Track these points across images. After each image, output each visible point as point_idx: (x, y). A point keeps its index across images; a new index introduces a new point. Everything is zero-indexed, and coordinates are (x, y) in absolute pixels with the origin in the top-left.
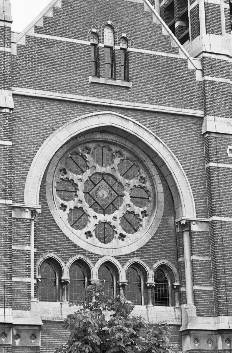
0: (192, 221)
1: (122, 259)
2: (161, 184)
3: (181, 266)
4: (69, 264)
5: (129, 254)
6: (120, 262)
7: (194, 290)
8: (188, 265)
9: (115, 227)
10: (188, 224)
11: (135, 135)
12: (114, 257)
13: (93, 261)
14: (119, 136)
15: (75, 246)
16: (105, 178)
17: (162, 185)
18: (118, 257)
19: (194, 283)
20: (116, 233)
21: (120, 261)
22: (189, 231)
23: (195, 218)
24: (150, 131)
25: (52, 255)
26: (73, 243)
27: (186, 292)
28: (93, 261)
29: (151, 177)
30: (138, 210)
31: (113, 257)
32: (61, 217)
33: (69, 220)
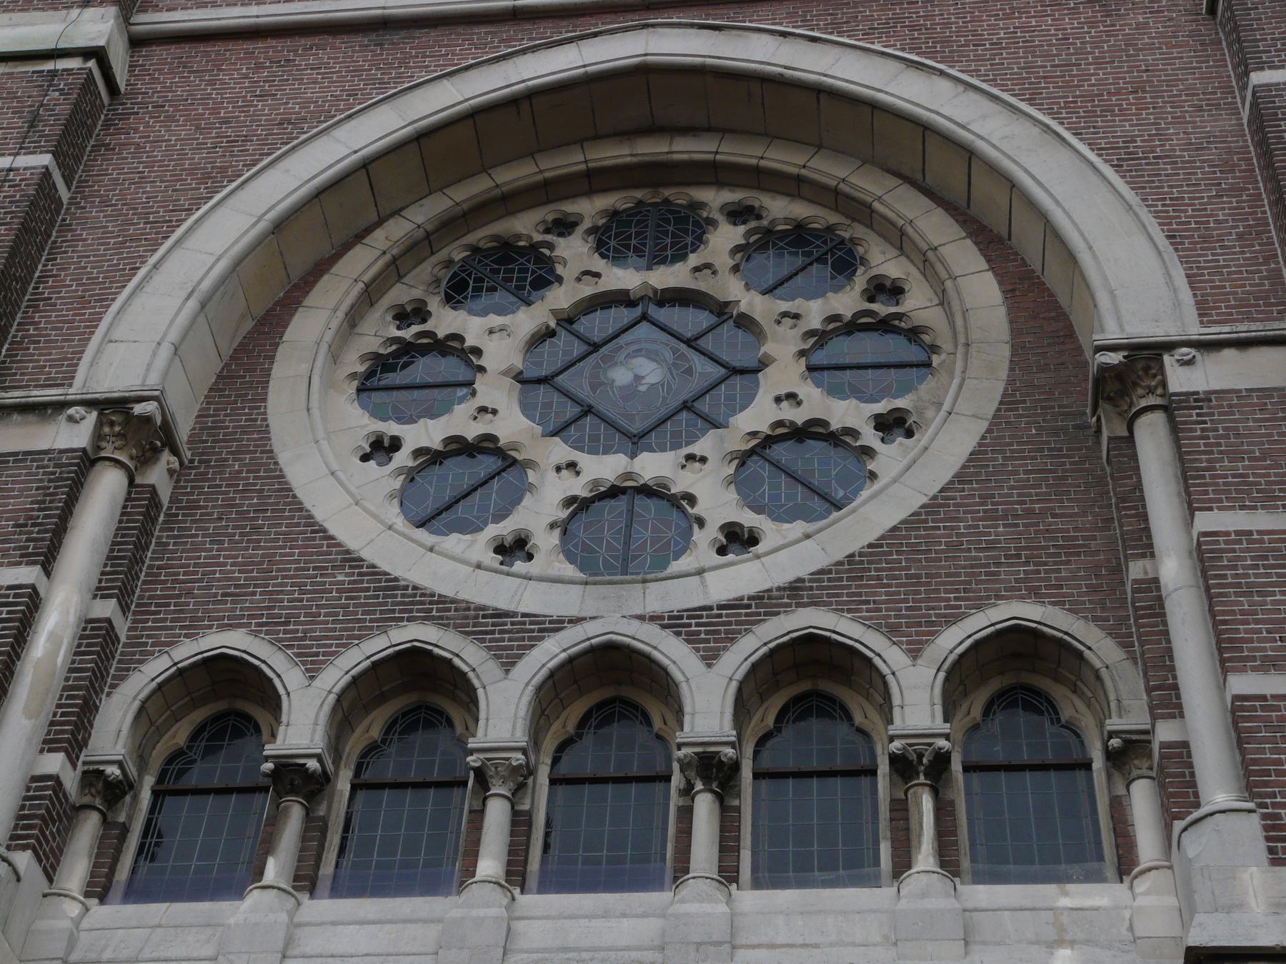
0: (1170, 346)
1: (707, 628)
2: (990, 274)
3: (1142, 620)
4: (335, 676)
5: (762, 598)
6: (688, 641)
7: (1237, 698)
8: (1173, 568)
9: (691, 499)
10: (1146, 357)
11: (782, 75)
12: (653, 618)
13: (499, 648)
14: (733, 131)
15: (391, 585)
16: (654, 311)
17: (996, 275)
18: (681, 617)
19: (1228, 654)
20: (701, 522)
21: (687, 634)
22: (1164, 408)
23: (1195, 330)
24: (877, 47)
25: (235, 641)
26: (386, 574)
27: (1185, 745)
28: (499, 648)
29: (926, 261)
30: (847, 413)
31: (641, 618)
32: (335, 466)
33: (403, 498)
